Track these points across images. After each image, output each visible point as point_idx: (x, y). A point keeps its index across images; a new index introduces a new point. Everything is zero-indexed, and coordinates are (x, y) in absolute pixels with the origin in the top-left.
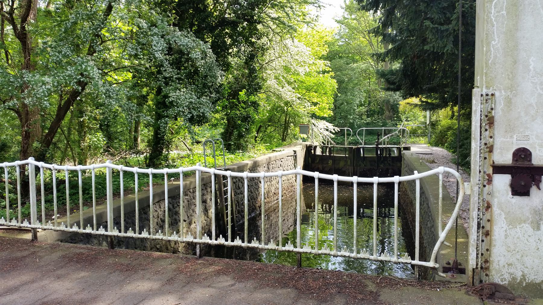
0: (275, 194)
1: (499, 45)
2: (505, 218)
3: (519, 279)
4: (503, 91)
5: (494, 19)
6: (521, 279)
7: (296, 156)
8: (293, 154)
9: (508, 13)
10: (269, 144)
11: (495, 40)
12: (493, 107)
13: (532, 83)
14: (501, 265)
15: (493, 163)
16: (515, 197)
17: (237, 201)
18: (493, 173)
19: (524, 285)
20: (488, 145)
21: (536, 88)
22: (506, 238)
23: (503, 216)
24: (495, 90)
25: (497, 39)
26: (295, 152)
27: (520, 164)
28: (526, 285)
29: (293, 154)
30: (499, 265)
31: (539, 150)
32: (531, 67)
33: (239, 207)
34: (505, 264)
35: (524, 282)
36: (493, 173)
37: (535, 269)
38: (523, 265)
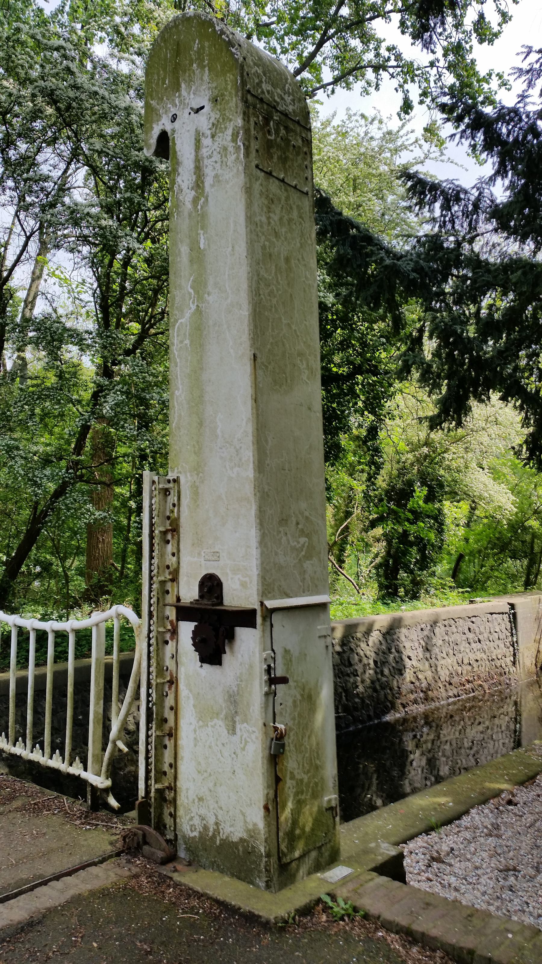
0: (450, 684)
1: (183, 397)
2: (194, 706)
3: (211, 829)
4: (188, 474)
5: (176, 353)
6: (214, 830)
7: (514, 615)
8: (507, 610)
9: (191, 342)
10: (468, 589)
11: (178, 389)
12: (176, 502)
13: (221, 458)
14: (191, 799)
15: (178, 599)
16: (205, 666)
17: (342, 687)
18: (178, 620)
19: (218, 842)
20: (171, 569)
21: (225, 467)
22: (195, 745)
23: (192, 702)
24: (180, 473)
25: (180, 387)
26: (512, 606)
27: (207, 604)
28: (220, 844)
29: (507, 610)
30: (187, 798)
31: (232, 579)
32: (219, 431)
33: (347, 700)
34: (195, 797)
35: (218, 838)
36: (178, 620)
37: (230, 813)
38: (217, 802)
